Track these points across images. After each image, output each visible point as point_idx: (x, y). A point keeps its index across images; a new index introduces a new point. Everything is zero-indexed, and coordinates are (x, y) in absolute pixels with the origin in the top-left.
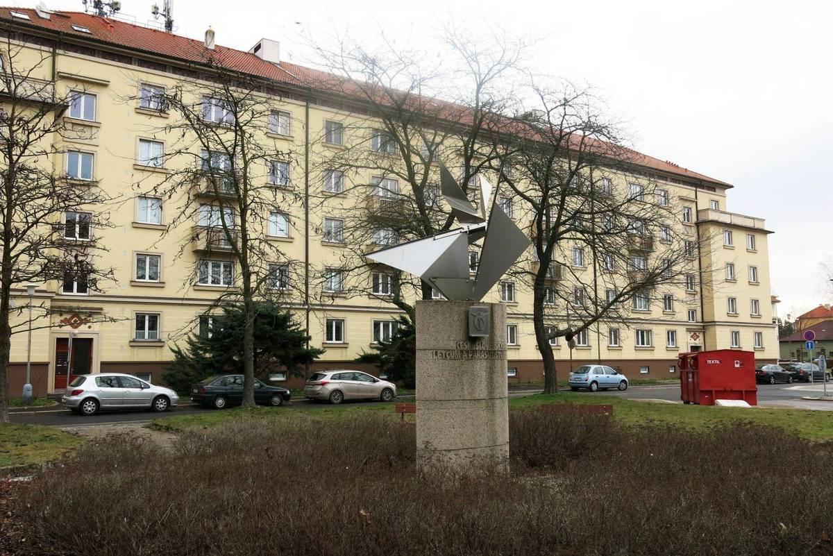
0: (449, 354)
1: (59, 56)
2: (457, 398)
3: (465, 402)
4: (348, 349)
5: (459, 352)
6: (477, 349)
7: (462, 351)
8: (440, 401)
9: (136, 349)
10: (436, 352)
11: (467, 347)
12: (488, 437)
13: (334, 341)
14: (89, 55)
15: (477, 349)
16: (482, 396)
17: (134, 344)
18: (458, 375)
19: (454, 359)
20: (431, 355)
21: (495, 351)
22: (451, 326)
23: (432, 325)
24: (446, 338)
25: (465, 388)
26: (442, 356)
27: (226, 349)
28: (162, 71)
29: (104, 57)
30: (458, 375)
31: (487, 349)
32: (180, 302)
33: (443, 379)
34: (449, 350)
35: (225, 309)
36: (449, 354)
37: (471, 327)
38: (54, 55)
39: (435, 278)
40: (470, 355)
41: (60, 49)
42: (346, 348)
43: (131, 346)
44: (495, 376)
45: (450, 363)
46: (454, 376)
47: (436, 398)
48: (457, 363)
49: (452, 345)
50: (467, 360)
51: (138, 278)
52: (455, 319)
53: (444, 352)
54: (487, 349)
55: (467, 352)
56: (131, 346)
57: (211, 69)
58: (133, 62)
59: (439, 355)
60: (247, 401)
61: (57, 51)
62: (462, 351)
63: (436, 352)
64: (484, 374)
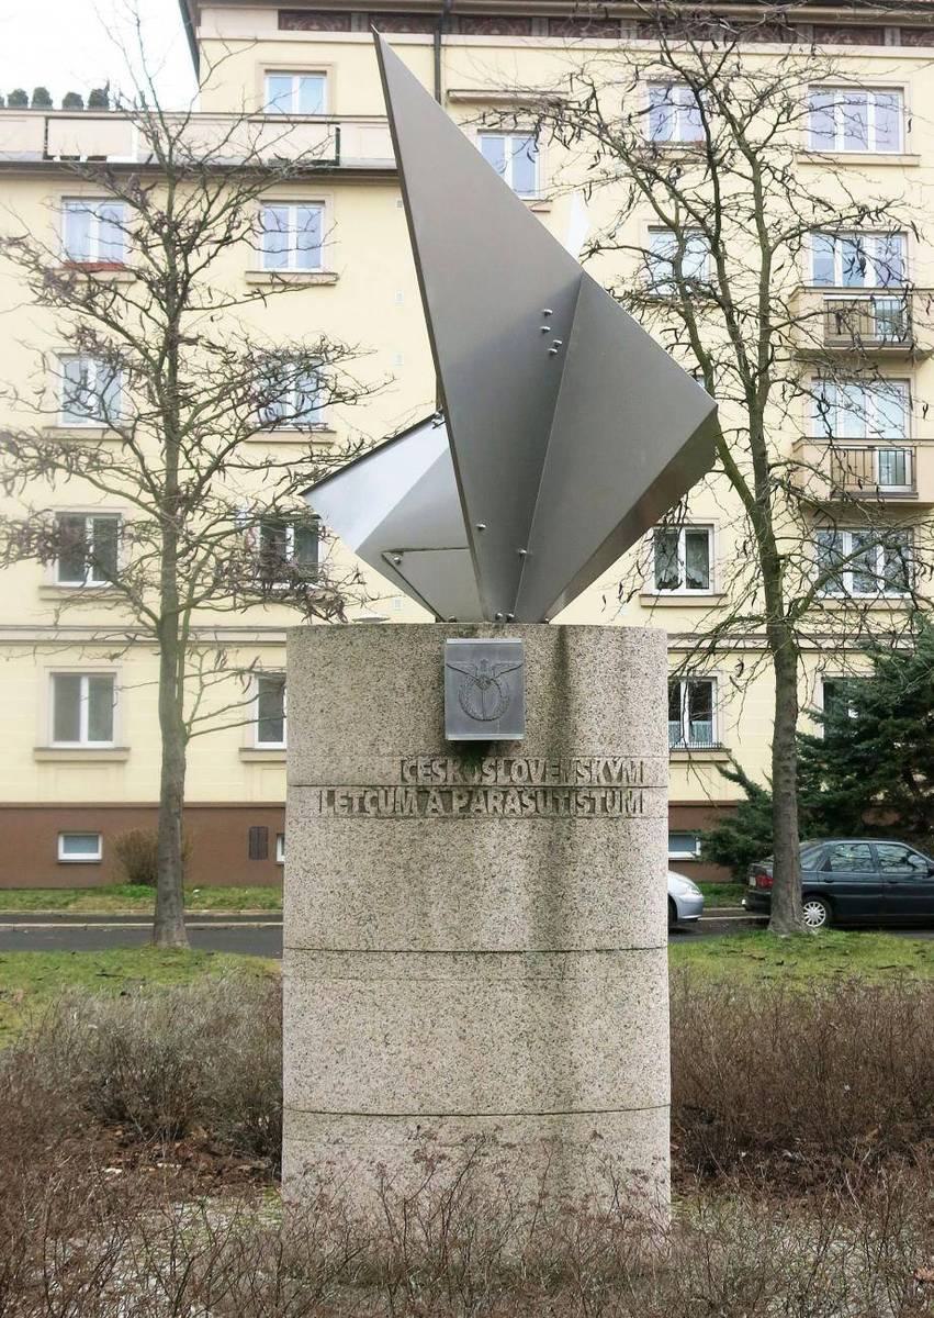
0: (374, 800)
1: (449, 50)
2: (403, 944)
3: (433, 959)
4: (127, 766)
5: (412, 793)
6: (488, 781)
7: (423, 791)
8: (342, 952)
9: (51, 769)
10: (331, 794)
11: (447, 774)
12: (532, 1081)
13: (85, 742)
14: (337, 30)
15: (488, 781)
16: (507, 942)
17: (44, 757)
18: (407, 869)
19: (394, 816)
20: (314, 803)
21: (575, 790)
22: (383, 707)
23: (318, 706)
24: (361, 747)
25: (434, 912)
26: (351, 807)
27: (865, 768)
28: (875, 44)
29: (553, 32)
30: (407, 869)
31: (537, 781)
32: (252, 637)
33: (352, 882)
34: (373, 787)
35: (876, 660)
36: (374, 800)
37: (453, 709)
38: (437, 47)
39: (400, 552)
40: (456, 804)
41: (450, 32)
42: (122, 762)
43: (246, 762)
44: (572, 875)
45: (378, 828)
46: (391, 873)
47: (329, 943)
48: (403, 830)
49: (386, 768)
50: (444, 819)
51: (662, 585)
52: (401, 683)
53: (356, 794)
54: (537, 781)
55: (446, 793)
56: (246, 762)
57: (637, 17)
58: (888, 40)
59: (339, 801)
60: (782, 916)
61: (445, 39)
62: (423, 791)
63: (331, 794)
64: (518, 869)
